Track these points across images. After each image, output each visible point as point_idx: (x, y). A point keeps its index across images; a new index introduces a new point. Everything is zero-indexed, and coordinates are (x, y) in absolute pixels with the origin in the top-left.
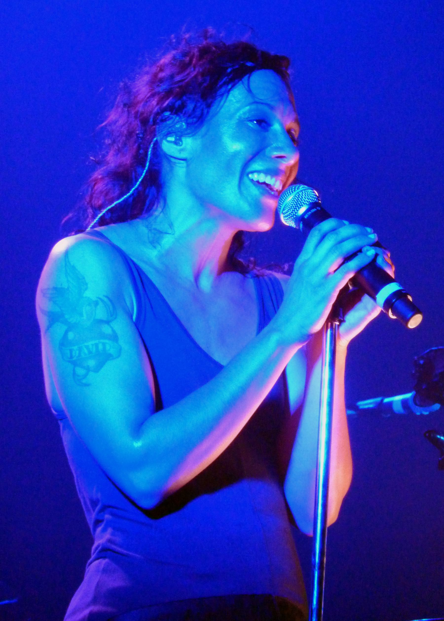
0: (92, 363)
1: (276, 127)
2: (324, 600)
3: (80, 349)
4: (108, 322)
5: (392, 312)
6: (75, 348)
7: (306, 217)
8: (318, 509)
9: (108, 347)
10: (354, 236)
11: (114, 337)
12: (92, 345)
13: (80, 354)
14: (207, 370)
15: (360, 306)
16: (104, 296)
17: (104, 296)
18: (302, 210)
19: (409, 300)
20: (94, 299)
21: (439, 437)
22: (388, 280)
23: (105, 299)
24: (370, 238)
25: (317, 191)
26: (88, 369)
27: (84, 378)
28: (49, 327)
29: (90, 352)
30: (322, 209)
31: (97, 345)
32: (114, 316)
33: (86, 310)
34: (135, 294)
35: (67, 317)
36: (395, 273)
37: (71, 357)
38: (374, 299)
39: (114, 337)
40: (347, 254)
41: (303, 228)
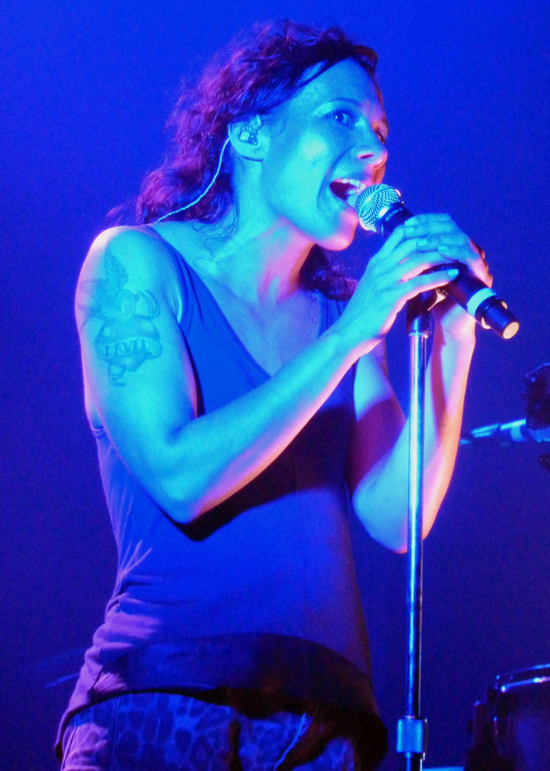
0: (128, 361)
1: (361, 123)
3: (117, 346)
4: (149, 319)
5: (485, 320)
6: (112, 345)
7: (387, 219)
9: (147, 345)
11: (155, 335)
12: (131, 342)
18: (383, 212)
19: (503, 307)
20: (135, 293)
22: (481, 285)
23: (147, 294)
25: (399, 191)
26: (124, 368)
27: (118, 378)
28: (84, 324)
29: (127, 350)
31: (135, 343)
32: (157, 313)
33: (125, 303)
34: (182, 294)
37: (107, 354)
38: (465, 307)
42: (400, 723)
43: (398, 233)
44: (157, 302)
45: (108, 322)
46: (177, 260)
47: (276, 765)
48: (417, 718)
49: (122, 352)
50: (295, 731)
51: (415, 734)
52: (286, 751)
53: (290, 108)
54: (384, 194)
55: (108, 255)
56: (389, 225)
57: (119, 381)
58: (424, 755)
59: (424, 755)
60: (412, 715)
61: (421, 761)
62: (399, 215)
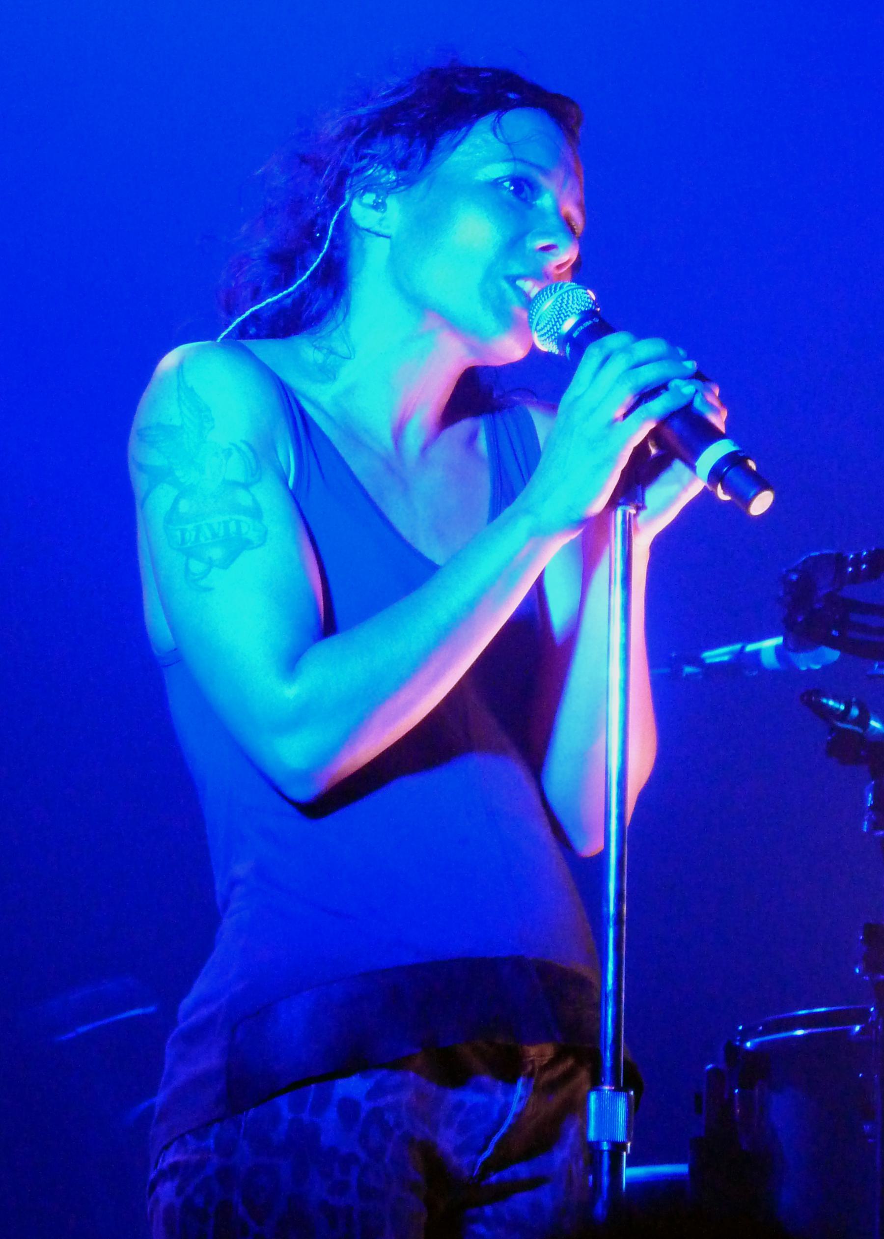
0: (216, 553)
2: (626, 978)
3: (198, 529)
4: (246, 486)
5: (723, 488)
6: (190, 527)
7: (575, 335)
8: (610, 817)
9: (244, 528)
10: (659, 359)
11: (256, 513)
12: (219, 523)
13: (197, 537)
14: (409, 573)
15: (666, 477)
16: (242, 441)
17: (242, 441)
18: (568, 325)
19: (750, 469)
21: (825, 701)
22: (712, 435)
23: (244, 448)
24: (685, 367)
25: (594, 292)
26: (211, 564)
27: (202, 578)
29: (215, 535)
30: (602, 320)
31: (226, 524)
35: (178, 474)
36: (727, 423)
38: (693, 468)
39: (256, 513)
40: (646, 387)
41: (570, 354)
42: (593, 1097)
43: (593, 355)
44: (258, 462)
45: (184, 492)
46: (286, 394)
47: (481, 1160)
48: (618, 1089)
49: (207, 539)
50: (507, 1106)
51: (614, 1114)
52: (496, 1138)
53: (446, 162)
54: (570, 298)
55: (182, 385)
56: (577, 344)
57: (203, 583)
58: (629, 1144)
59: (629, 1144)
60: (610, 1085)
61: (625, 1153)
62: (595, 327)
